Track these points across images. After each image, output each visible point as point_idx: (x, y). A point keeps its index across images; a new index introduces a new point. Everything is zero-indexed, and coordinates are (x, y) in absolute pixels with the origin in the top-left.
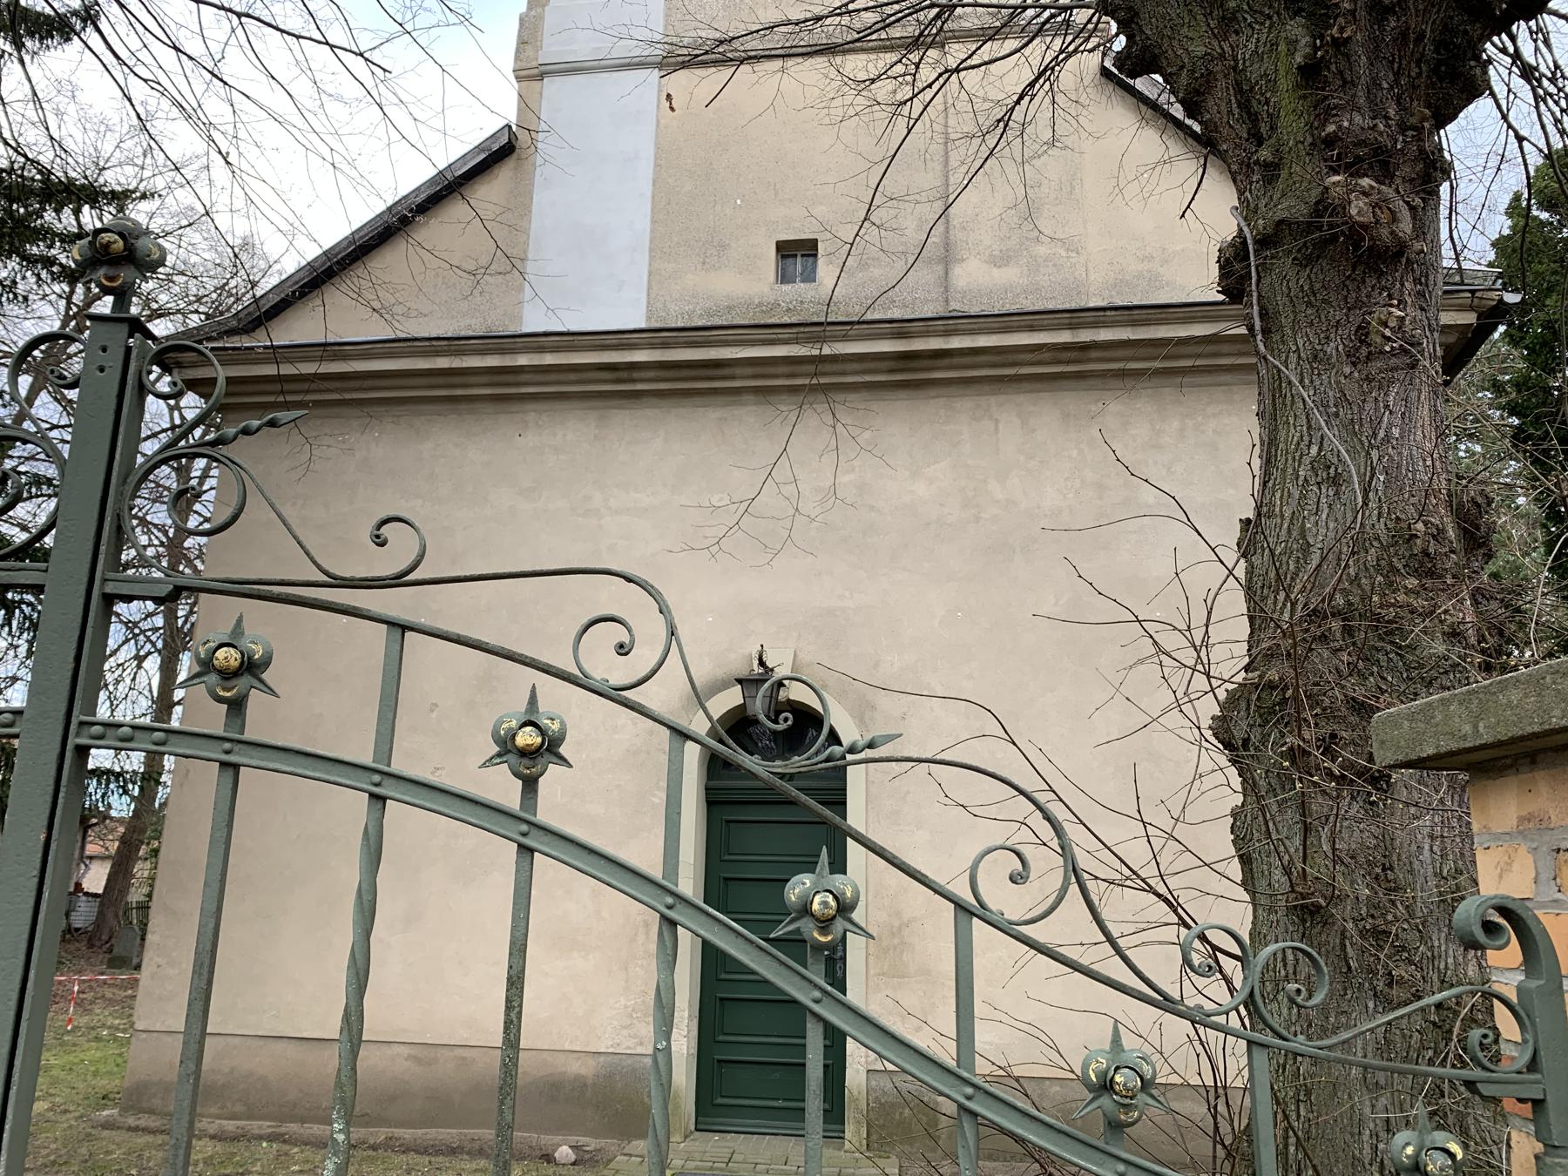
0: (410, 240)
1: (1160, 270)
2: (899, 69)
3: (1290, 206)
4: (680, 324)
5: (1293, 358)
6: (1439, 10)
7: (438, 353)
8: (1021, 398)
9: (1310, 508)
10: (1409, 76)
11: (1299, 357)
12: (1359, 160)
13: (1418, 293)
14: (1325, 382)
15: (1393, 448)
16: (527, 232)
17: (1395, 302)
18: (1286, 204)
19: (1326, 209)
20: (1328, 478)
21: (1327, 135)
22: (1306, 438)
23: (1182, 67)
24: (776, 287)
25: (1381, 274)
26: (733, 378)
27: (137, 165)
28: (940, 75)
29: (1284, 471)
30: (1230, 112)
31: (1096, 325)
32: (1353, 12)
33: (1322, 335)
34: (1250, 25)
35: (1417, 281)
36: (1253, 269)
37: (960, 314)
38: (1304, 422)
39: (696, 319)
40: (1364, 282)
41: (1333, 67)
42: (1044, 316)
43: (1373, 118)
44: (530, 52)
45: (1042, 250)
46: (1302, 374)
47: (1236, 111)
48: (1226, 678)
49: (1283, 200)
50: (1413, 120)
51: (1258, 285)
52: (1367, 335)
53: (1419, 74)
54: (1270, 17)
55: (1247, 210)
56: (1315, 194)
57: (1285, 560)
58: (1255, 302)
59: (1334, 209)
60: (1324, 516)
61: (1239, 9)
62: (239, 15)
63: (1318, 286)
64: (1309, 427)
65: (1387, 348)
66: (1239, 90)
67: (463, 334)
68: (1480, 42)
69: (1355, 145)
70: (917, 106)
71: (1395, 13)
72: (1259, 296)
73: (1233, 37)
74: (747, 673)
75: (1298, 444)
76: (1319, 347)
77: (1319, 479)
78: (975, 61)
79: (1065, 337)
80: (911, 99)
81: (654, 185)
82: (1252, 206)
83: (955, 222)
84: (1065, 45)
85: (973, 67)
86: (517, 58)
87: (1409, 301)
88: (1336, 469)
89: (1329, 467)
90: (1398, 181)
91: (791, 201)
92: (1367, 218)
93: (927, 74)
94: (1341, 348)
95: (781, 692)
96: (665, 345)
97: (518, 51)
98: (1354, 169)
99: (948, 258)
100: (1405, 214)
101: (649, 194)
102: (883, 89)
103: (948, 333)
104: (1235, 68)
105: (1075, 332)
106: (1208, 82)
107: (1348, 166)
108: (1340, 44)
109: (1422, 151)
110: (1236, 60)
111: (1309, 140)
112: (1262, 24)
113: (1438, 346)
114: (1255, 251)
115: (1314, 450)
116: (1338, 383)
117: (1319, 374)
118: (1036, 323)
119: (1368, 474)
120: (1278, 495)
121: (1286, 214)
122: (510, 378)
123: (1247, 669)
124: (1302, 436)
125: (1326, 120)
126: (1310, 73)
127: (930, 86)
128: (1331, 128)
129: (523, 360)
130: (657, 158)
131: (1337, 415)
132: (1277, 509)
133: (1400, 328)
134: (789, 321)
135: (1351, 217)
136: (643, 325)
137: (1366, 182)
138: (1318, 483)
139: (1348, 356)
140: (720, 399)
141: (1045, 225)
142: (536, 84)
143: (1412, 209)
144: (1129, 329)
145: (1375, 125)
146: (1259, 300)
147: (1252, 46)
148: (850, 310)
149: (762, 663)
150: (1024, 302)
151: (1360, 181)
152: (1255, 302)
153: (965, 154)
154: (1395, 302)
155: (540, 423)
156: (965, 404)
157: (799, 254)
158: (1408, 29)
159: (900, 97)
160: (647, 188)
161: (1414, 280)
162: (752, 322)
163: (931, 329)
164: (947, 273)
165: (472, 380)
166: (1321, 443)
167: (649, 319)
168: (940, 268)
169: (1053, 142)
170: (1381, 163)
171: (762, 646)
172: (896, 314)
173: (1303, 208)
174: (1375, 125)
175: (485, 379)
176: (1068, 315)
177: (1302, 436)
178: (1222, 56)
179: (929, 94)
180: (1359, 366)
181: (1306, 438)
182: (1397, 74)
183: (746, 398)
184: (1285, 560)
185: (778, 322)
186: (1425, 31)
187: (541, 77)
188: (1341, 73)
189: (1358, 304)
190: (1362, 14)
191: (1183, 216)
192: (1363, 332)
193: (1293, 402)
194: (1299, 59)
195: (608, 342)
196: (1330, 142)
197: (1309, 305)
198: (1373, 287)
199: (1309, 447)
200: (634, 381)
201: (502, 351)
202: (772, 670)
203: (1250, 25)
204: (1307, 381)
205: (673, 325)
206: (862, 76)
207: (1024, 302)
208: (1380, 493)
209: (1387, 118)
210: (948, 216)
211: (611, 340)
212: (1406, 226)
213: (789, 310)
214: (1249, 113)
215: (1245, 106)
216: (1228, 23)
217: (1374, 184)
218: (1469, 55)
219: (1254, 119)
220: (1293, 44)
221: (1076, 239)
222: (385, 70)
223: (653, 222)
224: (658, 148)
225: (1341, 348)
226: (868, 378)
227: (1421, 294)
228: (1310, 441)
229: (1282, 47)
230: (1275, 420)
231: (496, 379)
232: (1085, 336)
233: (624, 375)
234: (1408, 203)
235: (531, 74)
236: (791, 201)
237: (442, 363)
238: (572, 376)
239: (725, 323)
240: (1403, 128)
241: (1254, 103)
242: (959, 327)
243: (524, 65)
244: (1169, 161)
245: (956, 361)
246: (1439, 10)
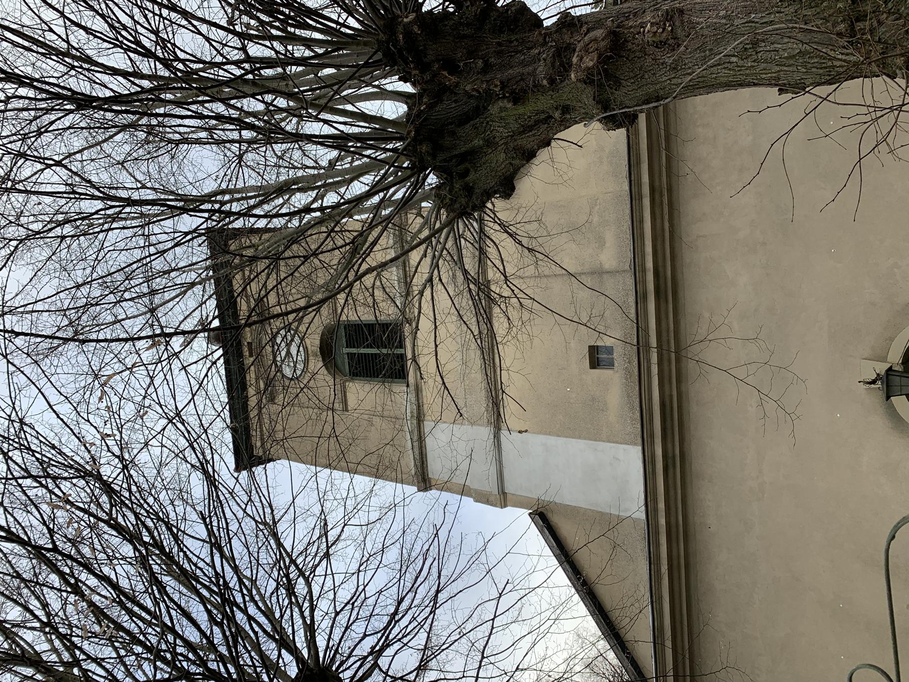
0: (596, 582)
1: (607, 152)
2: (503, 306)
3: (587, 96)
4: (639, 426)
5: (674, 81)
6: (486, 37)
7: (659, 571)
9: (773, 56)
10: (518, 46)
11: (674, 78)
12: (562, 65)
13: (634, 16)
14: (690, 60)
15: (733, 12)
16: (586, 510)
17: (642, 30)
18: (586, 100)
19: (589, 78)
20: (753, 48)
21: (548, 83)
22: (726, 65)
23: (511, 164)
24: (616, 369)
25: (626, 41)
26: (671, 396)
27: (144, 295)
28: (508, 286)
29: (747, 75)
30: (534, 135)
31: (640, 185)
32: (487, 82)
33: (661, 67)
34: (491, 132)
35: (628, 18)
36: (621, 111)
37: (632, 263)
38: (715, 68)
39: (636, 417)
40: (630, 49)
41: (514, 87)
42: (634, 215)
43: (539, 60)
44: (492, 499)
45: (596, 219)
46: (684, 75)
47: (533, 132)
48: (903, 93)
49: (583, 101)
50: (541, 40)
51: (631, 107)
52: (661, 42)
53: (517, 40)
54: (488, 122)
55: (587, 118)
56: (579, 85)
57: (810, 65)
58: (640, 108)
59: (589, 74)
60: (779, 46)
61: (484, 139)
62: (483, 657)
63: (631, 74)
64: (719, 65)
65: (670, 28)
66: (523, 132)
67: (647, 554)
68: (498, 10)
69: (554, 68)
70: (520, 295)
71: (488, 60)
72: (636, 106)
73: (497, 139)
74: (881, 393)
75: (730, 69)
76: (668, 68)
77: (754, 53)
78: (501, 268)
79: (647, 202)
80: (518, 298)
81: (559, 436)
82: (584, 116)
83: (580, 269)
85: (504, 269)
86: (495, 506)
87: (640, 21)
88: (747, 44)
89: (746, 49)
90: (572, 40)
91: (568, 361)
92: (595, 56)
93: (506, 293)
94: (668, 55)
95: (896, 369)
96: (652, 436)
97: (492, 505)
98: (566, 68)
99: (599, 272)
100: (592, 35)
101: (564, 439)
102: (514, 314)
103: (644, 270)
104: (512, 136)
105: (643, 196)
106: (518, 149)
107: (566, 71)
108: (503, 86)
109: (556, 32)
110: (508, 136)
111: (550, 92)
112: (491, 126)
114: (610, 111)
115: (734, 59)
116: (690, 53)
117: (685, 65)
118: (638, 220)
119: (750, 24)
120: (764, 76)
121: (591, 99)
122: (674, 530)
123: (893, 77)
124: (725, 68)
125: (541, 85)
126: (517, 98)
127: (513, 291)
128: (545, 82)
129: (662, 521)
130: (546, 434)
131: (711, 50)
132: (774, 75)
133: (657, 24)
134: (636, 362)
135: (594, 65)
136: (640, 448)
137: (575, 60)
138: (756, 53)
139: (674, 50)
141: (583, 218)
142: (509, 497)
143: (588, 31)
144: (642, 165)
145: (544, 59)
146: (640, 105)
147: (501, 129)
148: (629, 326)
149: (873, 382)
150: (625, 227)
151: (574, 63)
152: (640, 108)
153: (546, 268)
154: (642, 30)
155: (701, 514)
157: (597, 356)
158: (495, 51)
159: (517, 305)
160: (562, 440)
161: (627, 20)
162: (637, 383)
163: (641, 280)
164: (608, 272)
166: (729, 56)
167: (635, 444)
168: (605, 276)
169: (539, 221)
170: (563, 53)
171: (860, 382)
172: (632, 300)
174: (544, 59)
175: (674, 545)
176: (634, 201)
177: (725, 68)
178: (506, 144)
179: (516, 291)
180: (680, 42)
181: (726, 65)
182: (517, 52)
183: (683, 389)
184: (810, 65)
185: (637, 368)
186: (496, 43)
187: (504, 494)
188: (517, 82)
189: (643, 50)
190: (488, 77)
191: (581, 146)
192: (659, 45)
193: (703, 77)
194: (510, 105)
195: (651, 470)
196: (552, 81)
197: (642, 78)
198: (633, 44)
199: (731, 63)
200: (674, 457)
201: (657, 533)
202: (878, 375)
203: (491, 132)
204: (690, 71)
205: (639, 430)
206: (506, 325)
207: (625, 227)
208: (763, 15)
209: (539, 53)
210: (575, 273)
211: (649, 469)
212: (599, 33)
213: (629, 362)
214: (534, 126)
215: (531, 128)
216: (490, 143)
217: (576, 54)
218: (506, 15)
219: (537, 122)
220: (502, 109)
221: (590, 201)
222: (507, 583)
223: (580, 438)
224: (540, 433)
225: (668, 55)
227: (635, 14)
228: (728, 63)
229: (503, 114)
230: (713, 85)
232: (646, 190)
233: (670, 461)
234: (586, 34)
235: (502, 499)
236: (568, 361)
238: (672, 493)
239: (638, 399)
240: (545, 43)
241: (530, 123)
242: (640, 263)
243: (499, 502)
244: (552, 159)
245: (660, 263)
246: (486, 37)
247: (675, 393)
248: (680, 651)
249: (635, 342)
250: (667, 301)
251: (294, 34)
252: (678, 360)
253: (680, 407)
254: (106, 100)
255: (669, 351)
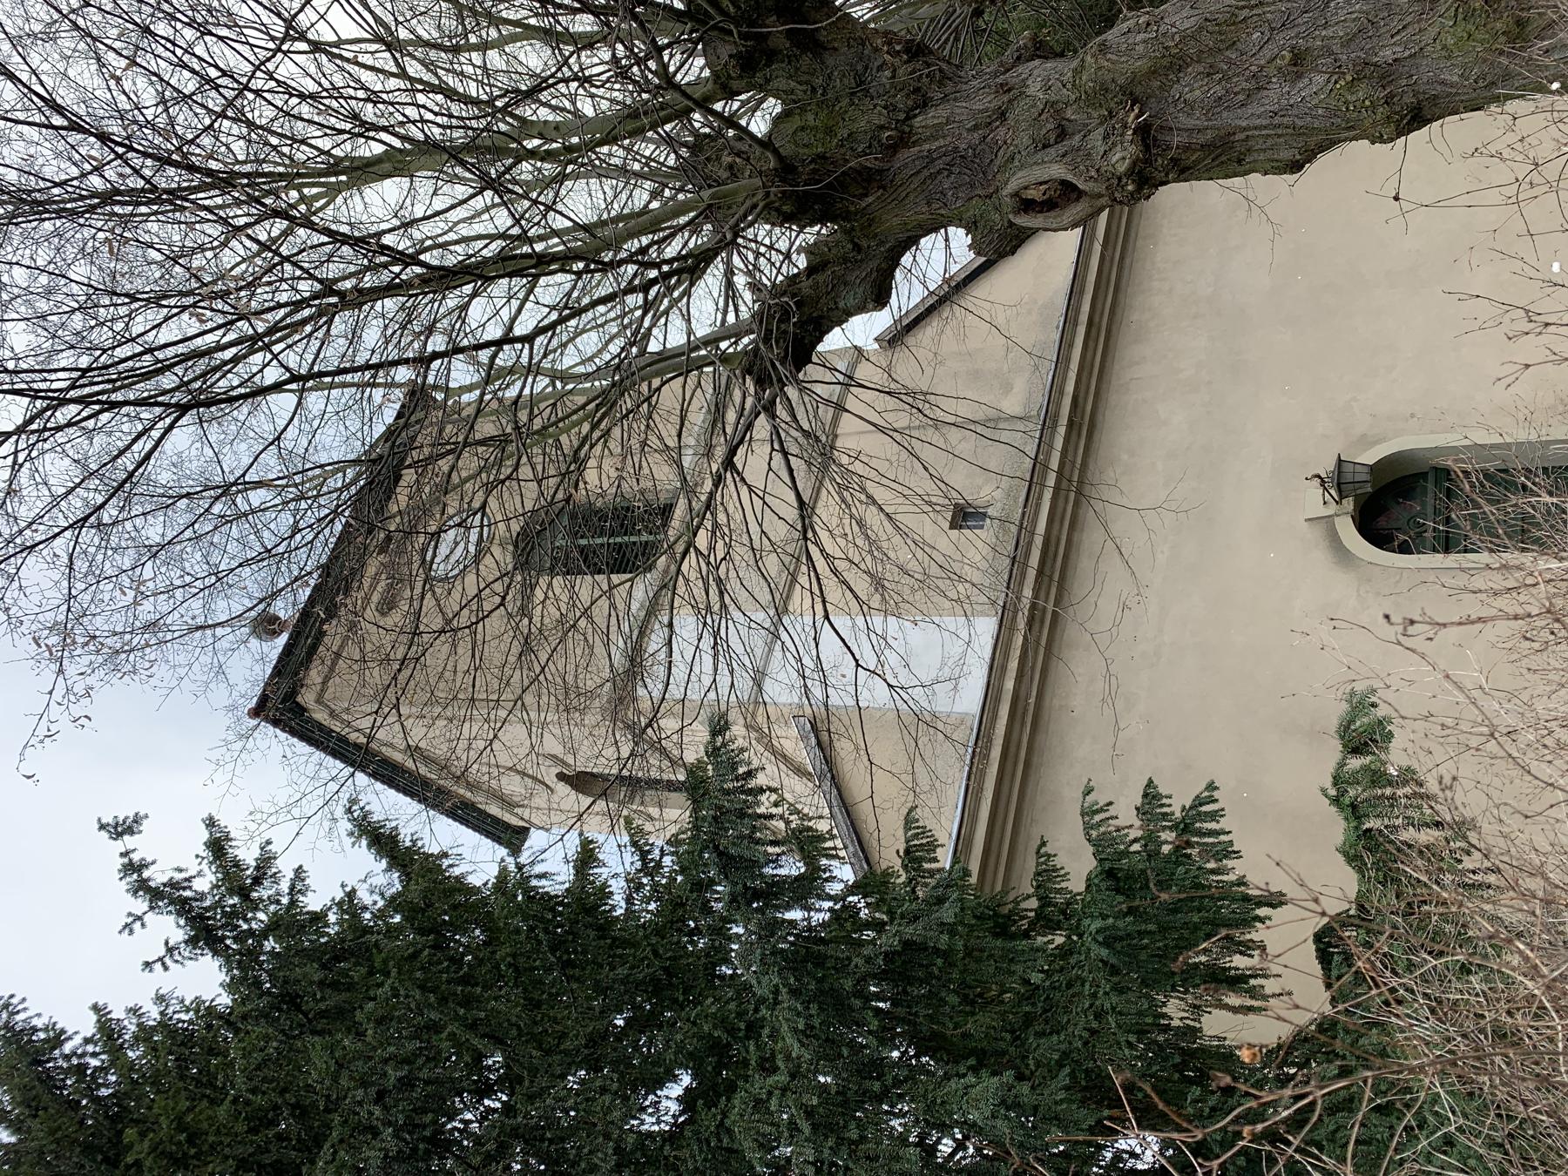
8: (1116, 367)
26: (1059, 540)
79: (1081, 330)
84: (78, 418)
103: (1062, 393)
113: (777, 364)
140: (1073, 556)
156: (1113, 398)
165: (1114, 228)
173: (1132, 149)
226: (1081, 451)
231: (1057, 519)
237: (996, 753)
247: (1064, 537)
248: (1051, 554)
249: (1055, 359)
250: (1079, 435)
251: (654, 232)
252: (1077, 504)
253: (1066, 557)
254: (156, 423)
255: (1073, 463)
